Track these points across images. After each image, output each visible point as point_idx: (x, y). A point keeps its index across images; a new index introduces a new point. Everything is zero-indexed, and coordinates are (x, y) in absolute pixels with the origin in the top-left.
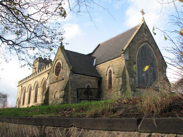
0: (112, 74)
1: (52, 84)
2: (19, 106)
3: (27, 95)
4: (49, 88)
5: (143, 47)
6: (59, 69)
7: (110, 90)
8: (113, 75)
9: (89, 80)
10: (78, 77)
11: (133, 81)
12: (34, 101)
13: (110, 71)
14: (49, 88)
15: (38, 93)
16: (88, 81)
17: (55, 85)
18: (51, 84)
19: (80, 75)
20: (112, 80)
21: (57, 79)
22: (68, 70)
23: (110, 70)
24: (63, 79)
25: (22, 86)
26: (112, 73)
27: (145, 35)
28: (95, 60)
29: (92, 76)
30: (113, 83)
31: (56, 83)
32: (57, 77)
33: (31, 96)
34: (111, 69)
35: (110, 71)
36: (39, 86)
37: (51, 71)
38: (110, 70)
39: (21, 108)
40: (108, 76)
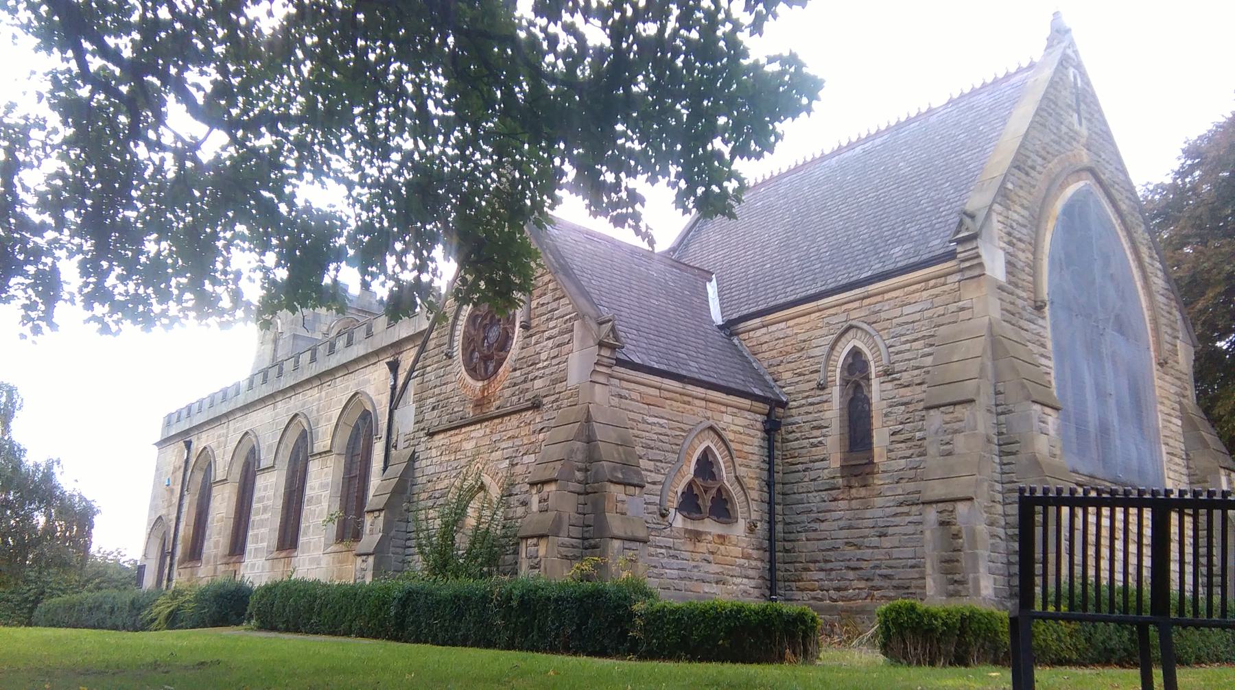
0: (875, 383)
1: (436, 438)
2: (159, 582)
3: (222, 505)
4: (413, 458)
5: (1069, 210)
6: (494, 334)
7: (863, 492)
8: (877, 391)
9: (709, 414)
10: (642, 388)
11: (1052, 432)
12: (275, 542)
13: (856, 362)
14: (413, 458)
15: (310, 491)
16: (707, 424)
17: (469, 446)
18: (431, 435)
19: (656, 380)
20: (876, 422)
21: (480, 403)
22: (576, 343)
23: (856, 353)
24: (536, 406)
25: (188, 445)
26: (873, 370)
27: (1077, 127)
28: (712, 289)
29: (729, 391)
30: (880, 438)
31: (478, 431)
32: (483, 389)
33: (255, 505)
34: (860, 345)
35: (856, 362)
36: (322, 442)
37: (431, 344)
38: (856, 353)
39: (1034, 567)
40: (836, 392)
